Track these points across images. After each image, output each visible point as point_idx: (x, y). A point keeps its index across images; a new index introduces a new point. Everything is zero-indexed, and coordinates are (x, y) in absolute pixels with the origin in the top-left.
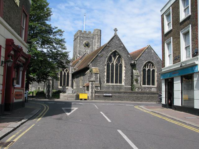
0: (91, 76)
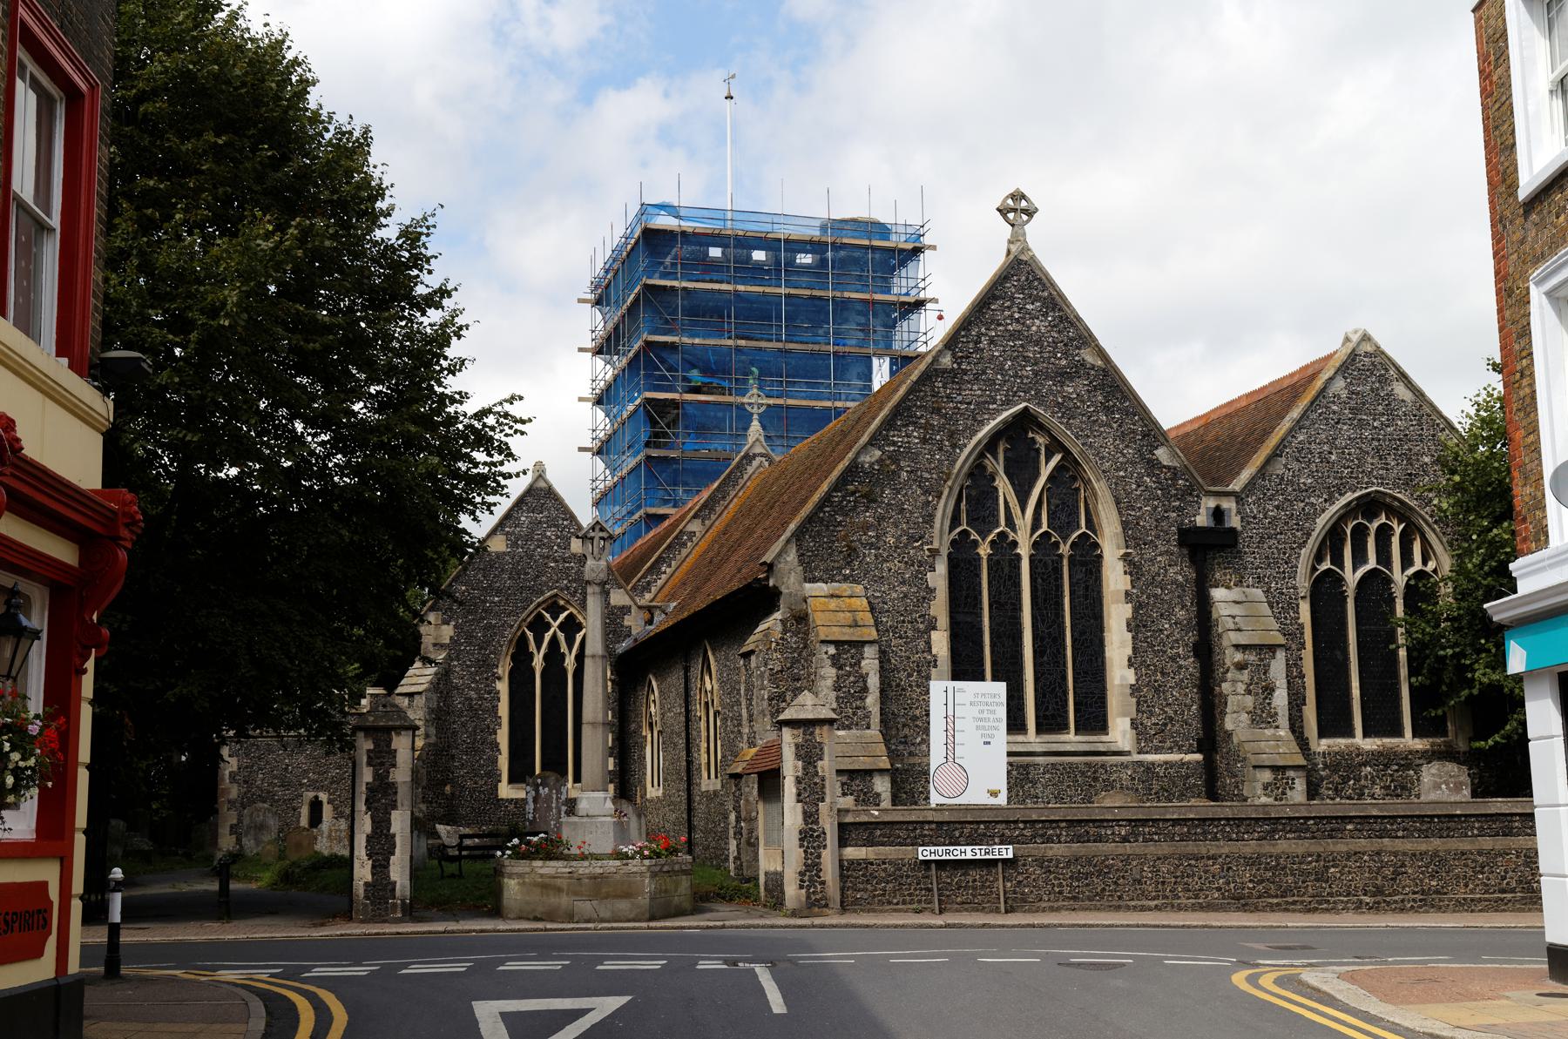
0: (794, 678)
